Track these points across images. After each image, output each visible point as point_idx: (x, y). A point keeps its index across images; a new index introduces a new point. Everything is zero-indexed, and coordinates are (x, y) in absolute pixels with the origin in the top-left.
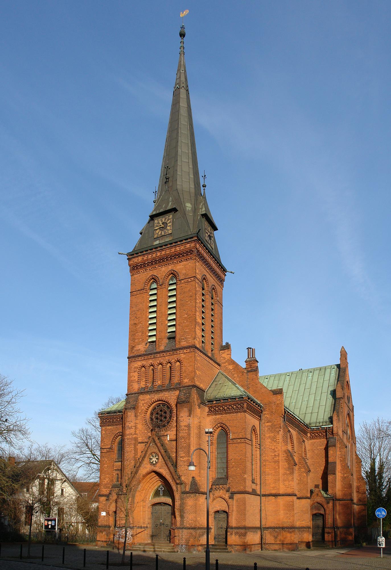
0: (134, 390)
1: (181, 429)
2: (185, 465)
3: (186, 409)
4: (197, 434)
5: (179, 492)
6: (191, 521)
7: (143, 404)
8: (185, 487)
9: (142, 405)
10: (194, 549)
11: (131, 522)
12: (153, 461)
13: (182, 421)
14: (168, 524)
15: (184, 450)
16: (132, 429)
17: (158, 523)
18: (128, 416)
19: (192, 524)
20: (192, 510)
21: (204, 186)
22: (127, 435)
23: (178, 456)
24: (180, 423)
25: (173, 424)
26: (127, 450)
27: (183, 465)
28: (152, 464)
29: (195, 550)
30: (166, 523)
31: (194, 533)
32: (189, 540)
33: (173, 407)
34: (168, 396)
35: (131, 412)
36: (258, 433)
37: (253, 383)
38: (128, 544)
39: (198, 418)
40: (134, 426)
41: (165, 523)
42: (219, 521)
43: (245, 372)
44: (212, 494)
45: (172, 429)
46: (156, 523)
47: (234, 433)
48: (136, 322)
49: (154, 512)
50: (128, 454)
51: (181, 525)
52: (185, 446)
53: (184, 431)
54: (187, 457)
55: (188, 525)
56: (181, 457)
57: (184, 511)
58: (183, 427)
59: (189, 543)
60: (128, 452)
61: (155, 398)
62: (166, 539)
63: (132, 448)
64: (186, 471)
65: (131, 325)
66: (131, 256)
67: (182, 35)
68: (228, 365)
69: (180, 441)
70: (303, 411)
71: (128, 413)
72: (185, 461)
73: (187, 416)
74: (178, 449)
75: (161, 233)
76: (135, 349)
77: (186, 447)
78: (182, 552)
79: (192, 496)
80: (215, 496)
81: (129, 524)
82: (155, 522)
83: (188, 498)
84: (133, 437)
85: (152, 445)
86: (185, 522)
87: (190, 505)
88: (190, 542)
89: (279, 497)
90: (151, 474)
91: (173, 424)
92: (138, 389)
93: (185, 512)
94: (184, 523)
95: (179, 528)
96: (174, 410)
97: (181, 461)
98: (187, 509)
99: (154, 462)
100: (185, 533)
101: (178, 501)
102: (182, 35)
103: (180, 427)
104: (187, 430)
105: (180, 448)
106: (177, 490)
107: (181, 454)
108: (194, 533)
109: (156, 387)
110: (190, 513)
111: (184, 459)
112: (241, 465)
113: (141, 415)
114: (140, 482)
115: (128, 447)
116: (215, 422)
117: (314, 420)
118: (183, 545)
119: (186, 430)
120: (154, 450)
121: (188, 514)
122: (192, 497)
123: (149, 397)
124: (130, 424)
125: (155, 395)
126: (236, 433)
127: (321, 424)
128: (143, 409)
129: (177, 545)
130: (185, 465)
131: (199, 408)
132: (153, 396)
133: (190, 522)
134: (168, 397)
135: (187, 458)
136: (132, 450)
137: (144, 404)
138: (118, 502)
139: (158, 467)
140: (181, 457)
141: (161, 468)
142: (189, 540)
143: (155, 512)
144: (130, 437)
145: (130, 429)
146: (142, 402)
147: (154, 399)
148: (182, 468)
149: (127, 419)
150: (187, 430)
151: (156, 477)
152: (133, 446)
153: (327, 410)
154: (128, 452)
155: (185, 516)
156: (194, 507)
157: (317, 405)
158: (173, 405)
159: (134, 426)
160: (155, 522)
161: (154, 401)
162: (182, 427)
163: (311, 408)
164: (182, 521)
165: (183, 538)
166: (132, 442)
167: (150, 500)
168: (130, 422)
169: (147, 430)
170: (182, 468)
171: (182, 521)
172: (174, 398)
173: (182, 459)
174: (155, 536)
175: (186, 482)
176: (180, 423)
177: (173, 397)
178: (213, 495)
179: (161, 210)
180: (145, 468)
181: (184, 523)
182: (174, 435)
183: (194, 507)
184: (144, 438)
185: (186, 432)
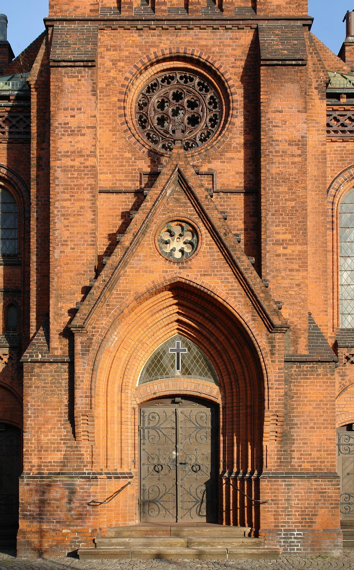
0: (78, 10)
1: (276, 152)
2: (291, 270)
3: (292, 88)
4: (317, 180)
5: (280, 357)
6: (318, 451)
7: (114, 62)
8: (295, 342)
9: (109, 64)
10: (333, 542)
11: (87, 458)
12: (173, 250)
13: (280, 124)
14: (200, 462)
15: (288, 222)
16: (84, 135)
17: (162, 462)
18: (62, 91)
19: (324, 462)
20: (322, 418)
22: (62, 156)
23: (266, 240)
24: (270, 130)
25: (231, 138)
26: (64, 207)
27: (285, 270)
28: (169, 257)
29: (338, 546)
30: (193, 462)
31: (331, 491)
32: (313, 515)
33: (231, 83)
34: (213, 46)
35: (77, 77)
38: (76, 535)
39: (318, 130)
40: (88, 127)
41: (191, 459)
42: (348, 454)
44: (339, 373)
45: (228, 155)
46: (155, 462)
49: (146, 425)
50: (66, 222)
51: (278, 466)
52: (292, 207)
53: (287, 160)
54: (300, 244)
55: (306, 466)
56: (278, 243)
57: (292, 420)
58: (281, 147)
59: (315, 522)
60: (69, 215)
61: (162, 45)
62: (194, 511)
63: (82, 204)
64: (296, 289)
69: (275, 190)
71: (66, 79)
72: (290, 255)
73: (299, 111)
74: (267, 214)
77: (297, 211)
78: (290, 553)
79: (320, 371)
80: (347, 378)
81: (80, 466)
82: (153, 459)
83: (307, 379)
84: (87, 163)
85: (170, 195)
86: (295, 455)
87: (314, 401)
88: (318, 520)
89: (69, 426)
90: (159, 296)
91: (231, 138)
92: (92, 8)
93: (296, 424)
94: (291, 458)
95: (276, 476)
96: (236, 93)
97: (278, 255)
98: (303, 412)
99: (178, 255)
100: (297, 493)
101: (275, 386)
103: (271, 145)
104: (300, 156)
105: (273, 215)
106: (271, 350)
107: (278, 233)
108: (331, 491)
109: (163, 8)
110: (312, 425)
111: (288, 251)
113: (105, 99)
114: (121, 316)
115: (67, 196)
116: (341, 160)
118: (294, 531)
119: (293, 156)
120: (179, 211)
121: (306, 428)
122: (319, 375)
123: (138, 38)
124: (73, 116)
125: (161, 36)
128: (115, 78)
129: (270, 531)
130: (291, 270)
131: (320, 99)
132: (155, 38)
133: (315, 454)
134: (213, 49)
135: (299, 248)
136: (81, 207)
137: (119, 61)
138: (30, 387)
139: (198, 271)
140: (278, 243)
141: (210, 275)
142: (313, 515)
143: (151, 425)
144: (76, 163)
145: (73, 133)
146: (109, 53)
147: (156, 50)
148: (283, 278)
149: (59, 98)
150: (300, 156)
151: (171, 308)
152: (88, 196)
154: (69, 215)
155: (295, 437)
156: (328, 406)
158: (233, 77)
159: (88, 127)
160: (153, 459)
161: (160, 54)
162: (278, 145)
164: (284, 451)
165: (292, 507)
166: (81, 182)
167: (137, 385)
168: (73, 109)
169: (133, 151)
170: (283, 278)
171: (284, 451)
172: (234, 52)
173: (280, 250)
174: (154, 502)
175: (298, 327)
176: (270, 130)
177: (228, 51)
178: (341, 376)
180: (147, 270)
181: (291, 458)
182: (237, 173)
183: (328, 406)
184: (122, 177)
185: (293, 163)
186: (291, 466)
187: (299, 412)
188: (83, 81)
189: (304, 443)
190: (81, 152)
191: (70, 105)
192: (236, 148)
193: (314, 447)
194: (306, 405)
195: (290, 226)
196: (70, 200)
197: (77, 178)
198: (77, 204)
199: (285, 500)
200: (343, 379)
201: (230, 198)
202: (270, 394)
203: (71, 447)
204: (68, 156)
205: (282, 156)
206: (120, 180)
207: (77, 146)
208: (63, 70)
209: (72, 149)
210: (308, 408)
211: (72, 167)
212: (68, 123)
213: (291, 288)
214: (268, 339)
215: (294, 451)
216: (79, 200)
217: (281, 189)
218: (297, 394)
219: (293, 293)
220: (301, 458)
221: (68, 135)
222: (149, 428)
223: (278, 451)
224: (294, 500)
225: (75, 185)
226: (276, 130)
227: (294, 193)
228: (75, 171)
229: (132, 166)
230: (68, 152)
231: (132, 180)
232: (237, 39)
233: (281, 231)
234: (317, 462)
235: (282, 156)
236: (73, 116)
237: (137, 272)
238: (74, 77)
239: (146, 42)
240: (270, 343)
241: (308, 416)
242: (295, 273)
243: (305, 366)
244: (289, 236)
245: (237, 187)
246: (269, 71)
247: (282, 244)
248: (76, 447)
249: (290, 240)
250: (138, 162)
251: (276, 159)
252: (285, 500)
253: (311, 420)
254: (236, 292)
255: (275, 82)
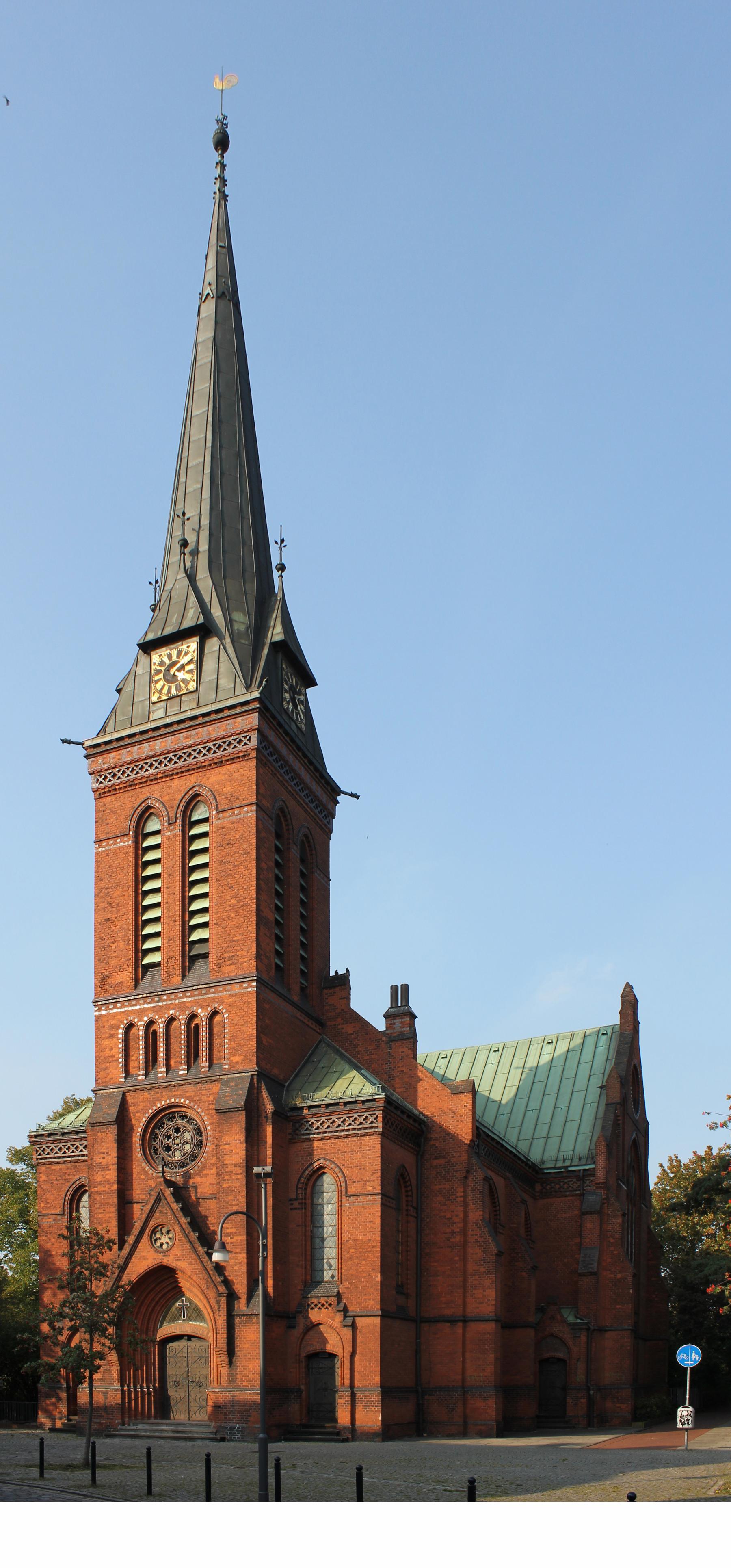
1: (226, 1172)
6: (253, 1374)
16: (110, 1170)
20: (256, 1352)
21: (282, 568)
26: (100, 1218)
34: (195, 1096)
36: (414, 1182)
37: (403, 1066)
43: (383, 1041)
45: (205, 1172)
47: (355, 1182)
48: (110, 916)
60: (102, 1223)
65: (98, 924)
66: (94, 751)
67: (222, 143)
68: (342, 1024)
70: (527, 1133)
75: (169, 691)
76: (110, 981)
82: (173, 1378)
86: (238, 1376)
94: (236, 1378)
102: (222, 143)
106: (219, 1308)
107: (228, 1228)
110: (249, 1356)
111: (233, 1240)
112: (370, 1255)
117: (551, 1153)
119: (237, 1174)
120: (162, 1219)
124: (104, 1158)
125: (162, 1092)
126: (358, 1182)
127: (567, 1163)
133: (251, 1376)
137: (137, 1113)
141: (181, 1260)
144: (106, 1189)
153: (582, 1130)
157: (560, 1118)
162: (227, 1167)
163: (546, 1127)
168: (104, 1153)
175: (241, 1291)
179: (168, 630)
180: (144, 1258)
181: (236, 1378)
185: (237, 1179)
186: (237, 1384)
187: (241, 1348)
188: (109, 1135)
189: (244, 1369)
190: (109, 1181)
191: (102, 1151)
192: (210, 1166)
193: (250, 1371)
194: (245, 1343)
195: (235, 1222)
196: (103, 1213)
197: (107, 1198)
198: (108, 1215)
199: (231, 1406)
200: (306, 1321)
201: (206, 1202)
202: (218, 1337)
203: (106, 1370)
204: (101, 1185)
205: (230, 1175)
206: (138, 1194)
207: (106, 1177)
208: (98, 1128)
209: (104, 1179)
210: (247, 1346)
211: (104, 1191)
212: (101, 1163)
213: (236, 1265)
214: (217, 1301)
215: (237, 1374)
216: (108, 1213)
217: (230, 1198)
218: (239, 1336)
219: (237, 1268)
220: (242, 1379)
221: (102, 1170)
222: (170, 1357)
223: (228, 1374)
224: (236, 1406)
225: (106, 1203)
226: (226, 1157)
227: (238, 1200)
228: (106, 1194)
229: (145, 1184)
230: (101, 1182)
231: (145, 1194)
232: (210, 1089)
233: (229, 1227)
234: (252, 1381)
235: (230, 1175)
236: (104, 1158)
237: (139, 1259)
238: (104, 1132)
239: (153, 1098)
240: (218, 1303)
241: (247, 1351)
242: (238, 1255)
243: (244, 1318)
244: (234, 1230)
245: (210, 1194)
246: (222, 1116)
247: (230, 1236)
248: (109, 1370)
249: (235, 1233)
250: (149, 1181)
251: (226, 1177)
252: (231, 1406)
253: (248, 1353)
254: (197, 1271)
255: (226, 1124)
